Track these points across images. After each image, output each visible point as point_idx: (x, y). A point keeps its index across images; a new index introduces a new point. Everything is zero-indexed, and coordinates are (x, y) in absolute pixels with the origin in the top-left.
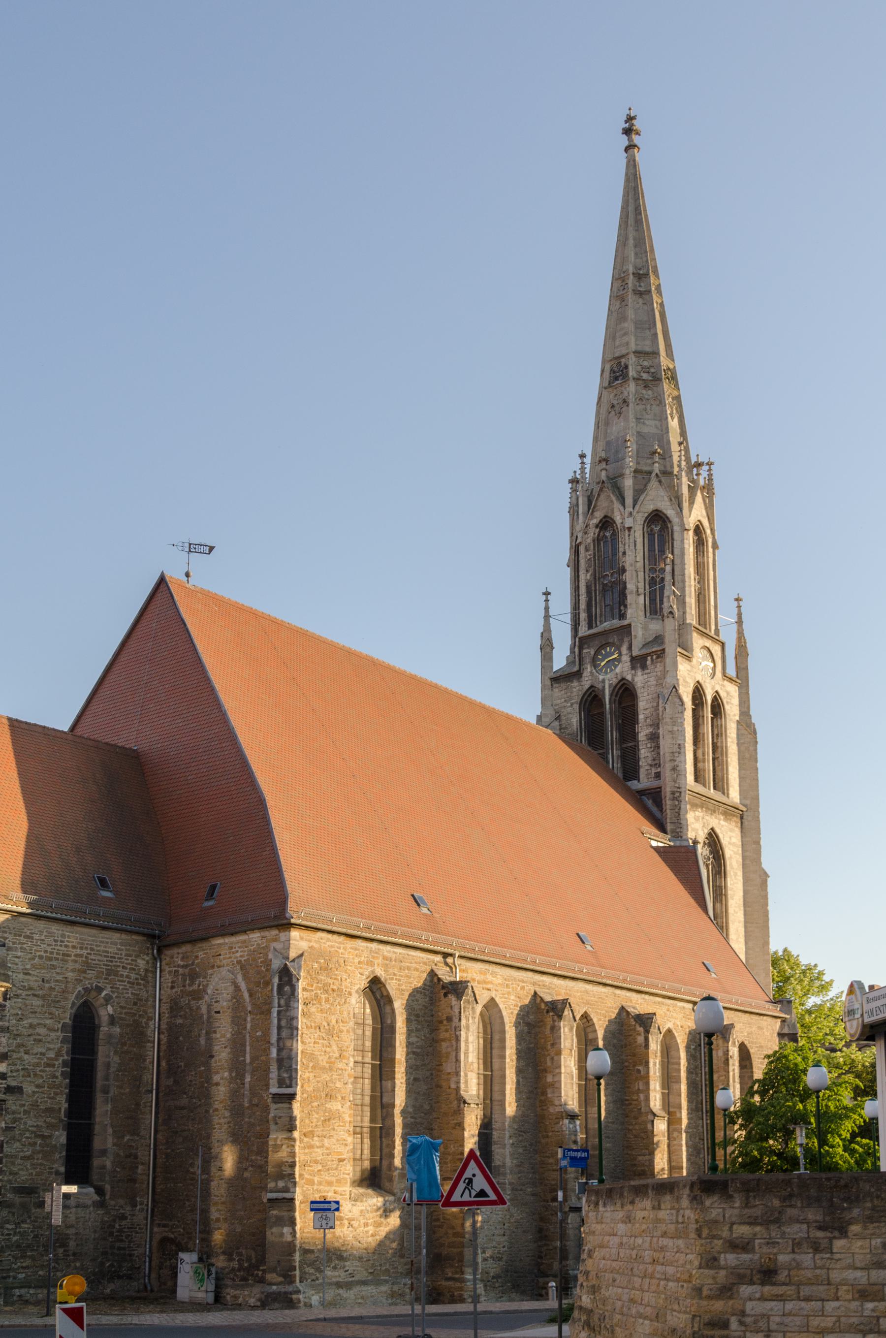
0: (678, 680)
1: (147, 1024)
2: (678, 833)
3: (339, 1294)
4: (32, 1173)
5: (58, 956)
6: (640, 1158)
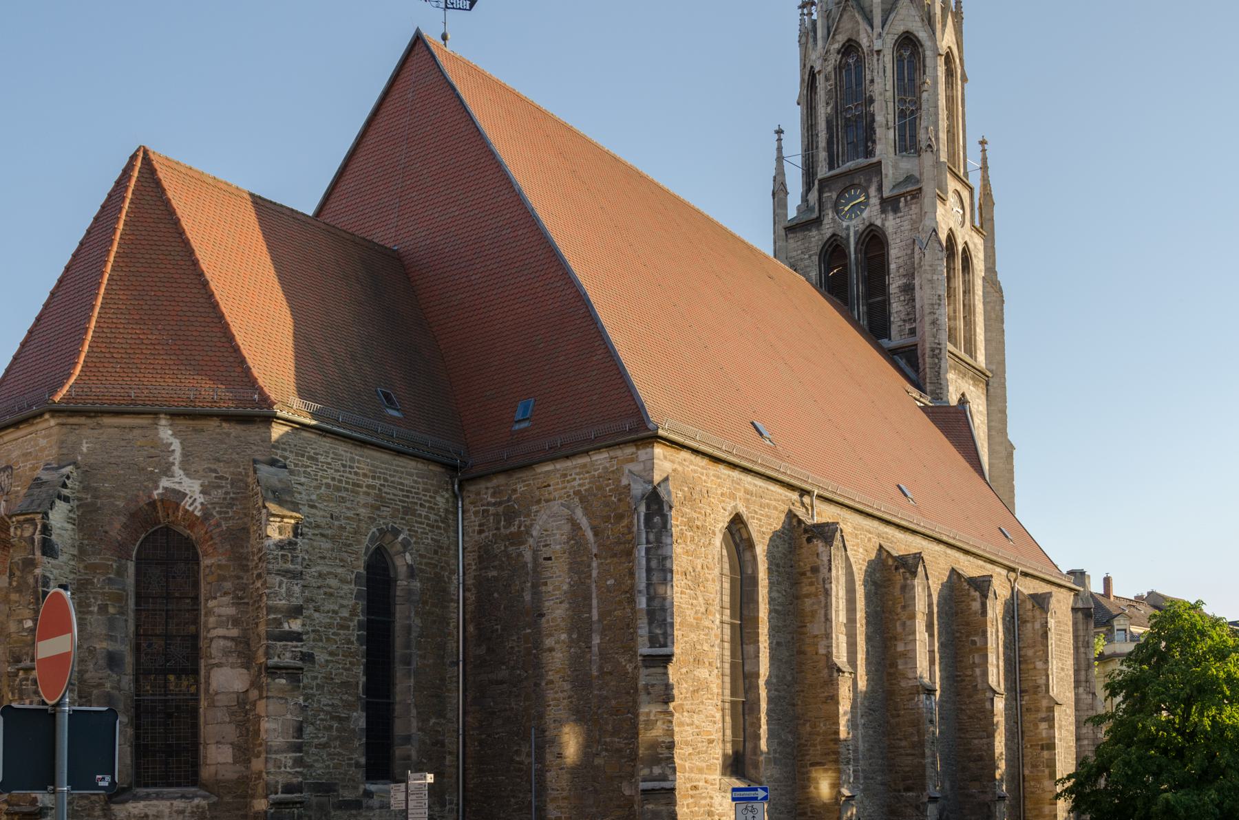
0: (937, 222)
1: (450, 578)
2: (937, 394)
4: (329, 765)
5: (347, 486)
6: (976, 741)
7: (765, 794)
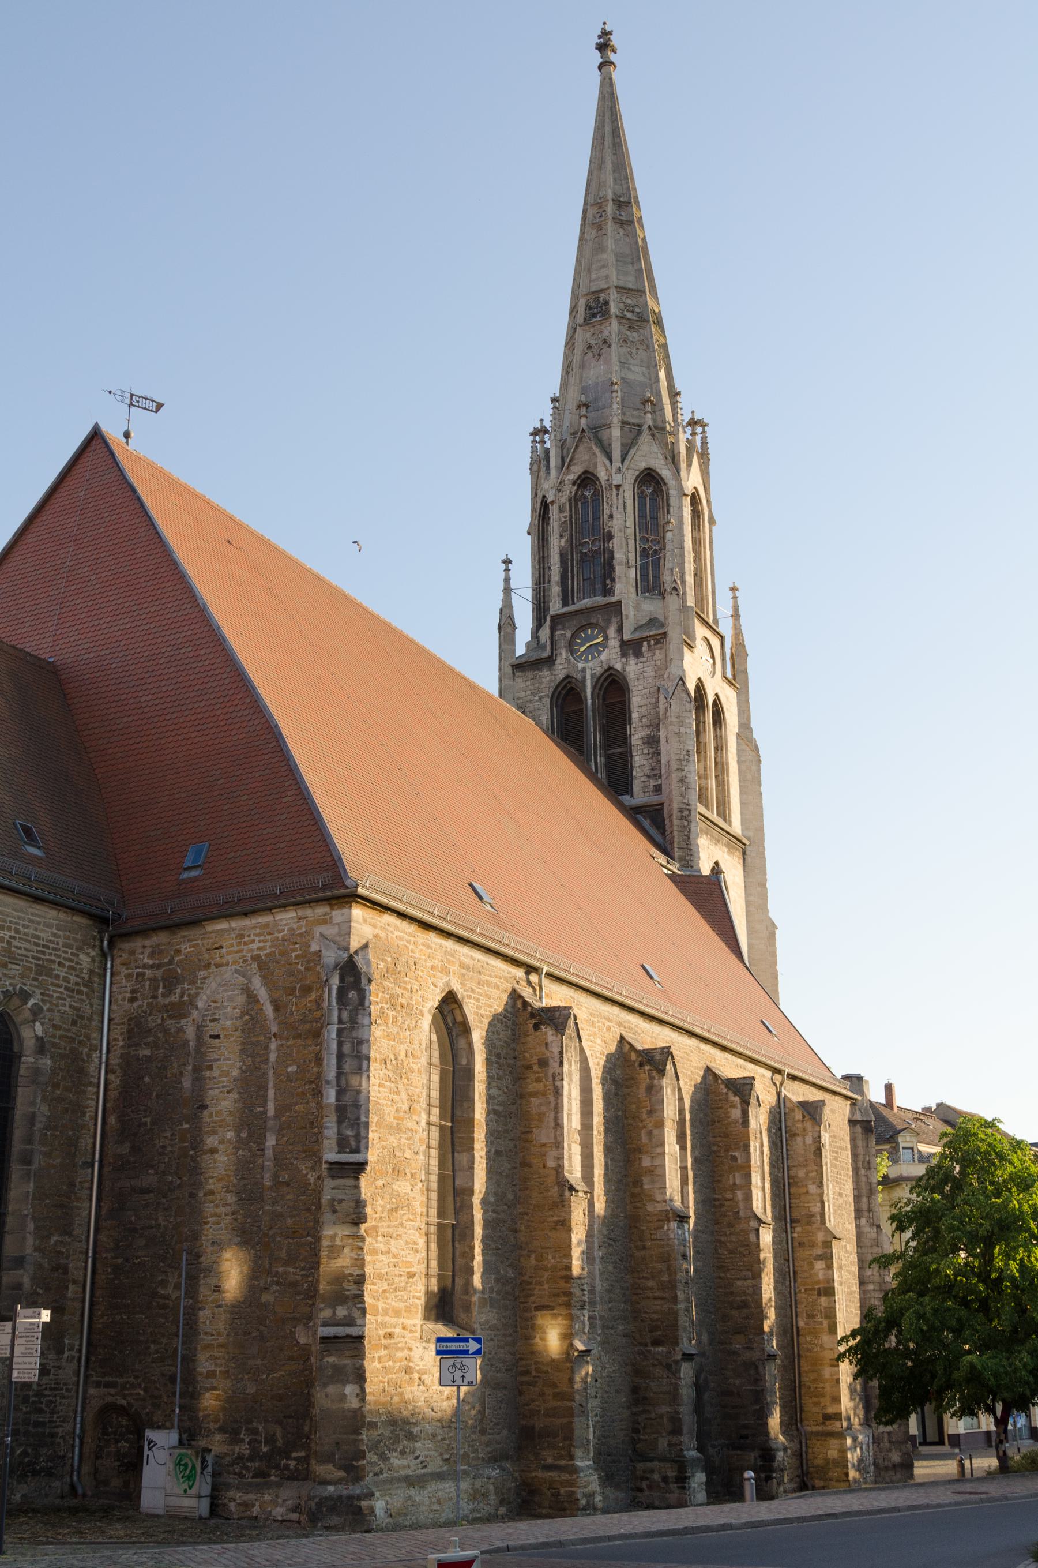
0: (684, 671)
1: (89, 1056)
3: (410, 1497)
6: (739, 1283)
7: (479, 1346)
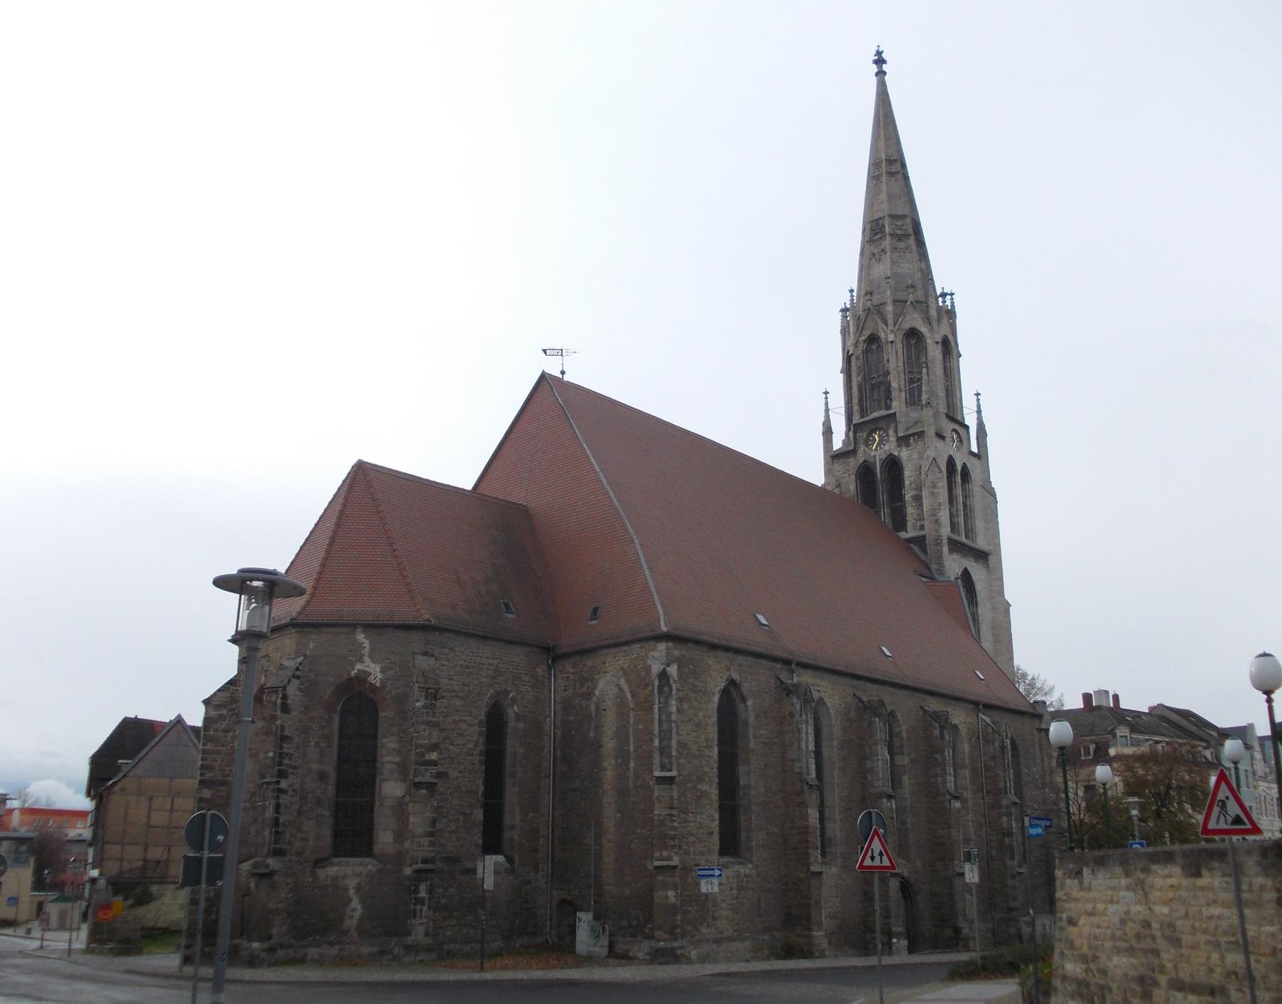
7: (720, 872)
